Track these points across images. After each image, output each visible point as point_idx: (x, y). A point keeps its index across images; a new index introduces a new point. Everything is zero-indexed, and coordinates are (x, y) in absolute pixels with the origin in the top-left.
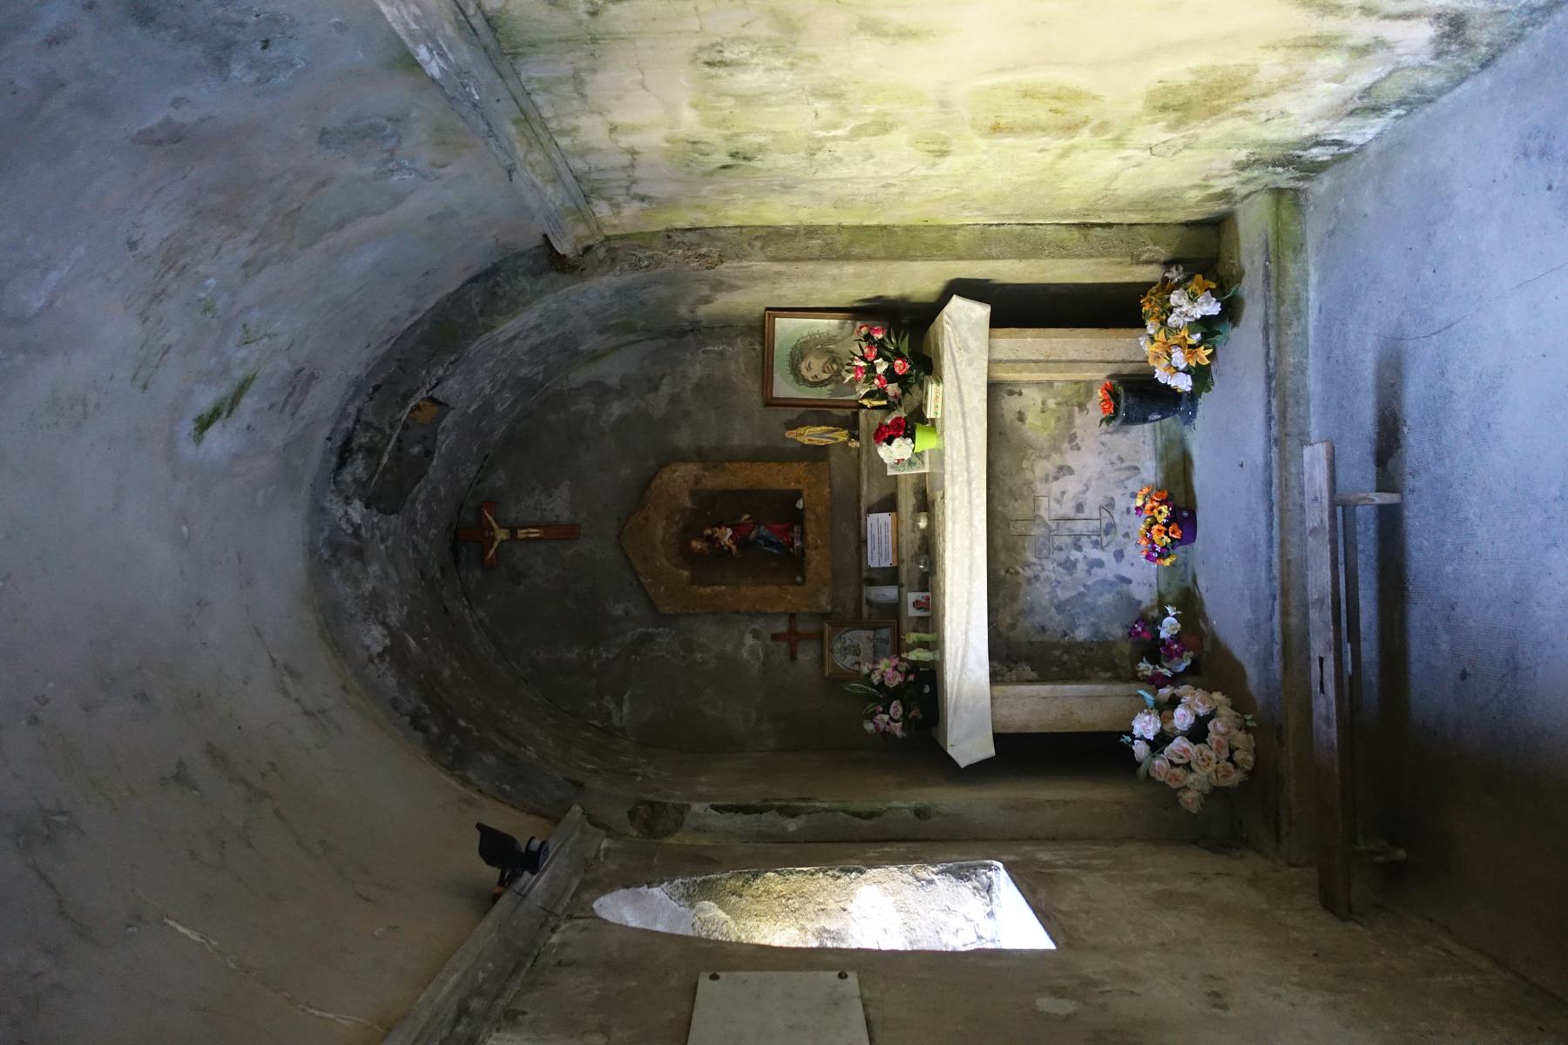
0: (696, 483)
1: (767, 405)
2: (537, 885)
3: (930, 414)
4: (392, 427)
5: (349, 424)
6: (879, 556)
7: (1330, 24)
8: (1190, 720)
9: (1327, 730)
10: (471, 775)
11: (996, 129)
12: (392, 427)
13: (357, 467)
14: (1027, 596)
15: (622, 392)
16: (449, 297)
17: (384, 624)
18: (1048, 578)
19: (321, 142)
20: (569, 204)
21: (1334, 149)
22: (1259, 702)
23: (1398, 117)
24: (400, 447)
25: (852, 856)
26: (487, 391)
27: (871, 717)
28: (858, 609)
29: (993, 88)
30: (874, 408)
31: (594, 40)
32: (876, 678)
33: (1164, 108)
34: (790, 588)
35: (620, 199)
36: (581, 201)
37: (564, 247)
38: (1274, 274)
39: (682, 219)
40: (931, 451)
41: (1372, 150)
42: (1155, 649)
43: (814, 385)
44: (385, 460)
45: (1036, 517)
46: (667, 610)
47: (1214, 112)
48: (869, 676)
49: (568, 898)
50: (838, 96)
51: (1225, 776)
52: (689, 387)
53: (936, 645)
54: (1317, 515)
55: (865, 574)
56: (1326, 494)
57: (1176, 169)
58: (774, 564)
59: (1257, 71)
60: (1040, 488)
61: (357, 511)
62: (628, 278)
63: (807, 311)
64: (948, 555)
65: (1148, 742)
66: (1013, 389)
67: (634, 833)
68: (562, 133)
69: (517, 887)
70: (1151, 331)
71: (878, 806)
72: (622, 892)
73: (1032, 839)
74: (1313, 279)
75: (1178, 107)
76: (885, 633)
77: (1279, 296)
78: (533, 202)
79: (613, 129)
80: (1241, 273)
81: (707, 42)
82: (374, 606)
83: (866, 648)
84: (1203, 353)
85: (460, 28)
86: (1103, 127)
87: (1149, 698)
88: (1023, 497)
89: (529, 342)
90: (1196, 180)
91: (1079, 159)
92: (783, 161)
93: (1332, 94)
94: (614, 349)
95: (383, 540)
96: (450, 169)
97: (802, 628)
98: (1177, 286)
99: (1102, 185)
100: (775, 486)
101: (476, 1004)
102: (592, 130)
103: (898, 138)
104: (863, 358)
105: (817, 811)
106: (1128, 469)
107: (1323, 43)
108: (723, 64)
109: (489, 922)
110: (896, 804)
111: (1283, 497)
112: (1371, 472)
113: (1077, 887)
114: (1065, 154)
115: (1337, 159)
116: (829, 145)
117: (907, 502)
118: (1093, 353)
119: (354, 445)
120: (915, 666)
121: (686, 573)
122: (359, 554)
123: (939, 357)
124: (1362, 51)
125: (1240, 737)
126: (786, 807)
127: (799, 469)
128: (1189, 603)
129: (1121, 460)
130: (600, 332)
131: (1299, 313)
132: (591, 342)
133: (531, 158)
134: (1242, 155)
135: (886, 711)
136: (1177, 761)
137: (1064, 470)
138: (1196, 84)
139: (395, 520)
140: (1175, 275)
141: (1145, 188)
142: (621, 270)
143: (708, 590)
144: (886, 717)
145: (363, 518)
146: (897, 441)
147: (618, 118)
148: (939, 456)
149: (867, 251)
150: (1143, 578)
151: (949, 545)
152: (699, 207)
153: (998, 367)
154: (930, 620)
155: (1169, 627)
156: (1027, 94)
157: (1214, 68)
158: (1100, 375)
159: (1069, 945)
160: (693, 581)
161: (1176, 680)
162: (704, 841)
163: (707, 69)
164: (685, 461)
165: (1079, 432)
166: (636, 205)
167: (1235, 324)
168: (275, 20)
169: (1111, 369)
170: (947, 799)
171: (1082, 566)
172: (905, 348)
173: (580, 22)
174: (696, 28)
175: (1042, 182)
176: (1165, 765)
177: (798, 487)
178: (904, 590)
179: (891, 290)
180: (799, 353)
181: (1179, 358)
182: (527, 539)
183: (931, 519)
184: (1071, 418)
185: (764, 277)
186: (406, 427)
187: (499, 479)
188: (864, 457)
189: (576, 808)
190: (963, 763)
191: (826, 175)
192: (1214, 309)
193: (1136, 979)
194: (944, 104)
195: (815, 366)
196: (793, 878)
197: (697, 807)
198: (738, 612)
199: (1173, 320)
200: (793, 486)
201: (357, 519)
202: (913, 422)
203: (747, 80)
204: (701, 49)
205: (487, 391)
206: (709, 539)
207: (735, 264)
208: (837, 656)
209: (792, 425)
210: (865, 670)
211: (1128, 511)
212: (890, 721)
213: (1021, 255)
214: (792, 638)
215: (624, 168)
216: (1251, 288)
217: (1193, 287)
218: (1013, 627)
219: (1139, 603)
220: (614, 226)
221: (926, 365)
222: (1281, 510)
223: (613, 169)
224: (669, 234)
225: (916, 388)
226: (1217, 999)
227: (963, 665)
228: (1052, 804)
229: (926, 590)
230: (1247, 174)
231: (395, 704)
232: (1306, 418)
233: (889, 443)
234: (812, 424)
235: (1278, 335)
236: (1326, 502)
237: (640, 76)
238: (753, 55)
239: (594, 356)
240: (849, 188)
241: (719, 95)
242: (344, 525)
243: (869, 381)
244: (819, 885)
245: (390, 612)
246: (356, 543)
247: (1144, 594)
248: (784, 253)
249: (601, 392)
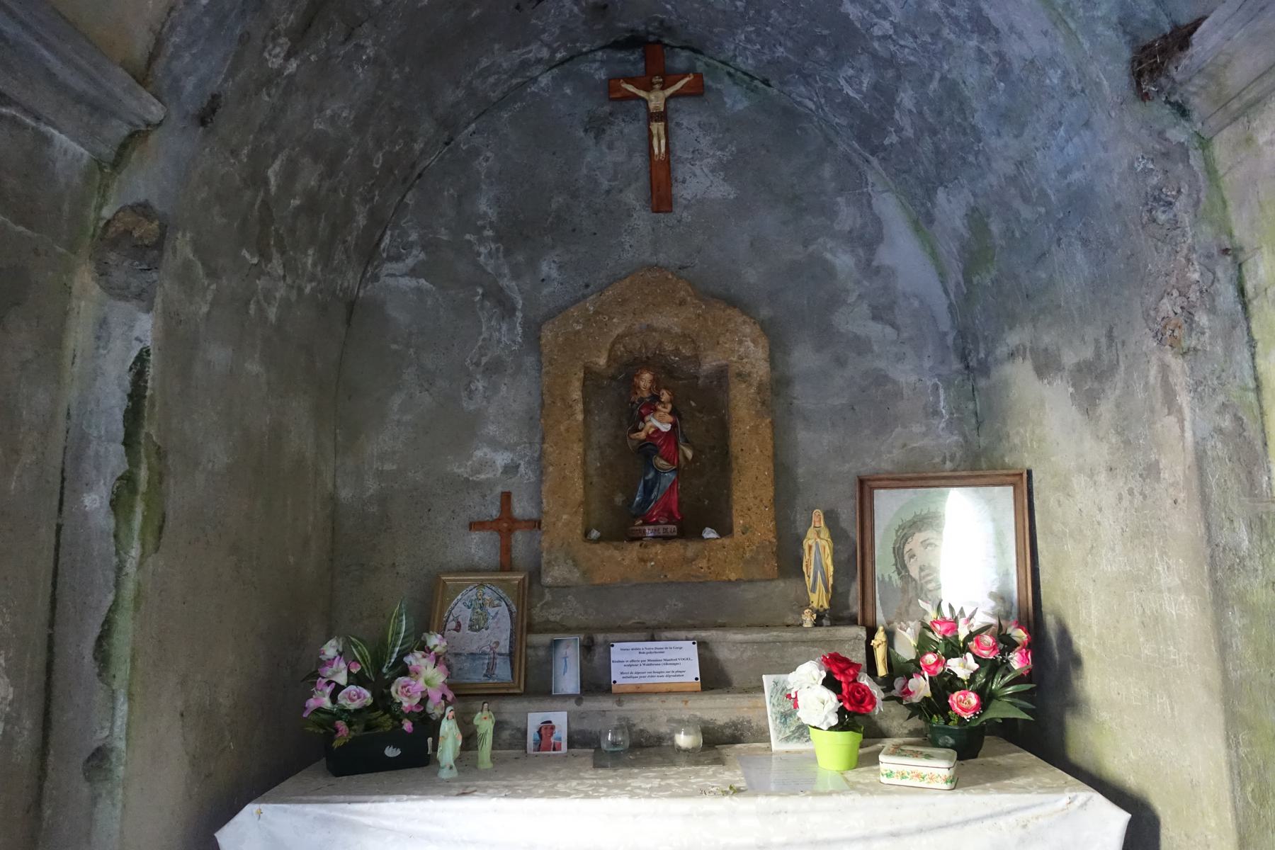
0: (739, 375)
1: (862, 482)
6: (630, 661)
15: (870, 269)
28: (547, 628)
34: (579, 520)
40: (812, 758)
43: (898, 553)
46: (547, 334)
48: (423, 647)
52: (881, 364)
53: (470, 775)
55: (600, 638)
58: (619, 499)
67: (107, 213)
71: (122, 671)
76: (503, 672)
94: (934, 255)
100: (736, 495)
117: (720, 709)
120: (428, 726)
121: (602, 361)
126: (133, 491)
143: (577, 394)
144: (342, 679)
146: (831, 699)
148: (800, 779)
149: (1238, 642)
160: (590, 376)
164: (772, 360)
172: (1000, 711)
177: (737, 530)
178: (572, 705)
183: (693, 757)
187: (736, 101)
188: (788, 635)
197: (146, 327)
198: (543, 440)
200: (738, 522)
206: (656, 398)
208: (472, 594)
209: (831, 519)
210: (434, 640)
229: (571, 743)
234: (835, 553)
249: (868, 239)
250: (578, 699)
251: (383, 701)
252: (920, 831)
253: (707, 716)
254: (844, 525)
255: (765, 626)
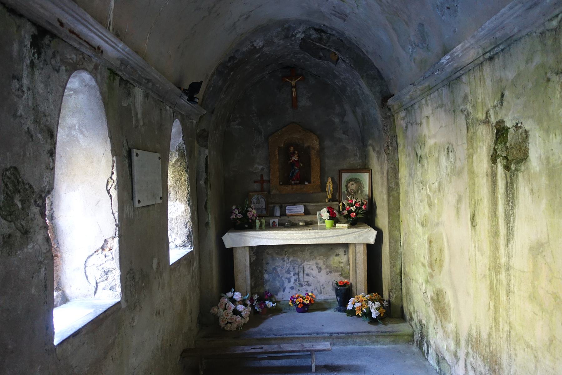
2: (184, 101)
3: (337, 225)
4: (329, 46)
5: (329, 32)
6: (289, 209)
7: (463, 343)
8: (240, 310)
9: (239, 350)
10: (215, 77)
11: (430, 242)
12: (329, 46)
13: (315, 35)
14: (278, 258)
16: (373, 63)
17: (263, 46)
18: (284, 265)
19: (420, 24)
20: (404, 103)
21: (426, 351)
22: (247, 332)
23: (436, 370)
24: (322, 49)
25: (193, 202)
26: (342, 77)
27: (237, 208)
29: (443, 239)
30: (339, 206)
31: (454, 111)
32: (250, 209)
33: (438, 295)
35: (406, 120)
36: (405, 107)
37: (390, 102)
38: (386, 334)
39: (400, 141)
40: (325, 226)
41: (426, 363)
42: (262, 300)
43: (346, 186)
44: (318, 44)
45: (304, 260)
47: (437, 311)
48: (250, 207)
49: (179, 111)
50: (439, 190)
51: (222, 321)
53: (261, 229)
54: (308, 346)
55: (283, 205)
56: (314, 349)
57: (419, 304)
59: (449, 322)
60: (314, 262)
61: (300, 36)
62: (380, 122)
63: (372, 183)
64: (291, 232)
65: (233, 297)
66: (346, 252)
68: (426, 101)
69: (183, 94)
70: (366, 296)
71: (209, 210)
72: (181, 128)
73: (200, 261)
74: (384, 347)
75: (438, 300)
76: (264, 212)
77: (379, 336)
78: (404, 91)
79: (428, 117)
80: (386, 325)
81: (454, 147)
82: (269, 42)
83: (259, 206)
84: (360, 313)
85: (456, 68)
86: (432, 276)
87: (246, 297)
88: (311, 256)
89: (358, 90)
90: (416, 308)
91: (422, 270)
92: (419, 173)
93: (443, 347)
95: (291, 44)
96: (413, 64)
97: (265, 185)
98: (381, 304)
99: (414, 278)
101: (150, 85)
102: (427, 111)
103: (427, 210)
104: (356, 202)
105: (207, 190)
106: (321, 290)
107: (458, 342)
108: (448, 152)
109: (173, 87)
110: (210, 216)
111: (313, 338)
112: (322, 364)
113: (187, 273)
114: (423, 265)
115: (423, 353)
116: (424, 188)
117: (308, 218)
118: (359, 277)
119: (322, 34)
120: (254, 222)
122: (286, 37)
123: (356, 227)
124: (455, 355)
125: (235, 326)
127: (318, 182)
128: (277, 311)
129: (324, 288)
130: (362, 114)
131: (373, 343)
132: (359, 110)
133: (418, 90)
134: (424, 322)
135: (239, 213)
136: (227, 306)
137: (320, 270)
138: (445, 304)
139: (297, 48)
140: (385, 303)
141: (413, 292)
142: (383, 121)
143: (277, 153)
144: (237, 213)
145: (298, 38)
146: (328, 214)
147: (431, 119)
148: (324, 228)
149: (391, 202)
150: (285, 296)
151: (294, 232)
152: (404, 145)
153: (353, 246)
154: (269, 227)
155: (270, 304)
156: (441, 250)
157: (450, 309)
158: (352, 281)
159: (171, 269)
161: (252, 306)
162: (196, 154)
163: (446, 147)
164: (320, 144)
165: (333, 274)
166: (404, 125)
167: (369, 323)
168: (456, 11)
169: (354, 284)
170: (212, 233)
171: (288, 276)
172: (359, 216)
173: (459, 106)
174: (459, 144)
175: (414, 258)
176: (225, 302)
179: (379, 211)
180: (357, 181)
181: (358, 305)
182: (292, 92)
183: (302, 226)
184: (337, 271)
185: (382, 168)
186: (329, 51)
188: (322, 204)
189: (205, 112)
190: (223, 238)
191: (415, 187)
192: (374, 316)
193: (163, 289)
194: (438, 224)
195: (353, 186)
196: (186, 183)
197: (207, 151)
199: (370, 303)
201: (298, 36)
202: (334, 219)
203: (443, 161)
204: (452, 145)
205: (342, 77)
207: (386, 159)
209: (333, 179)
210: (252, 206)
211: (307, 291)
212: (236, 214)
213: (391, 253)
214: (262, 181)
215: (416, 121)
216: (381, 327)
217: (381, 309)
218: (268, 254)
219: (277, 295)
220: (397, 118)
221: (354, 223)
222: (309, 337)
223: (416, 118)
224: (395, 136)
225: (346, 220)
226: (158, 313)
227: (255, 237)
228: (211, 267)
230: (418, 324)
231: (237, 51)
232: (339, 345)
233: (327, 212)
235: (366, 336)
236: (312, 349)
237: (444, 125)
238: (451, 162)
239: (354, 112)
240: (411, 195)
241: (439, 152)
242: (295, 32)
243: (348, 205)
244: (184, 192)
245: (267, 48)
246: (290, 36)
247: (279, 296)
248: (390, 175)
249: (342, 115)
250: (280, 217)
251: (245, 216)
252: (342, 235)
253: (306, 220)
254: (336, 180)
255: (318, 202)
